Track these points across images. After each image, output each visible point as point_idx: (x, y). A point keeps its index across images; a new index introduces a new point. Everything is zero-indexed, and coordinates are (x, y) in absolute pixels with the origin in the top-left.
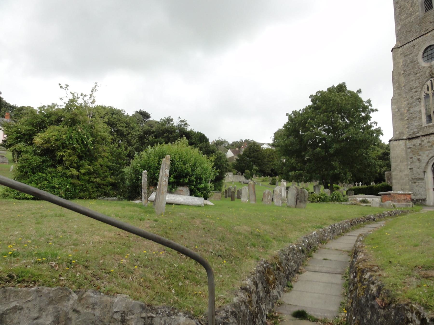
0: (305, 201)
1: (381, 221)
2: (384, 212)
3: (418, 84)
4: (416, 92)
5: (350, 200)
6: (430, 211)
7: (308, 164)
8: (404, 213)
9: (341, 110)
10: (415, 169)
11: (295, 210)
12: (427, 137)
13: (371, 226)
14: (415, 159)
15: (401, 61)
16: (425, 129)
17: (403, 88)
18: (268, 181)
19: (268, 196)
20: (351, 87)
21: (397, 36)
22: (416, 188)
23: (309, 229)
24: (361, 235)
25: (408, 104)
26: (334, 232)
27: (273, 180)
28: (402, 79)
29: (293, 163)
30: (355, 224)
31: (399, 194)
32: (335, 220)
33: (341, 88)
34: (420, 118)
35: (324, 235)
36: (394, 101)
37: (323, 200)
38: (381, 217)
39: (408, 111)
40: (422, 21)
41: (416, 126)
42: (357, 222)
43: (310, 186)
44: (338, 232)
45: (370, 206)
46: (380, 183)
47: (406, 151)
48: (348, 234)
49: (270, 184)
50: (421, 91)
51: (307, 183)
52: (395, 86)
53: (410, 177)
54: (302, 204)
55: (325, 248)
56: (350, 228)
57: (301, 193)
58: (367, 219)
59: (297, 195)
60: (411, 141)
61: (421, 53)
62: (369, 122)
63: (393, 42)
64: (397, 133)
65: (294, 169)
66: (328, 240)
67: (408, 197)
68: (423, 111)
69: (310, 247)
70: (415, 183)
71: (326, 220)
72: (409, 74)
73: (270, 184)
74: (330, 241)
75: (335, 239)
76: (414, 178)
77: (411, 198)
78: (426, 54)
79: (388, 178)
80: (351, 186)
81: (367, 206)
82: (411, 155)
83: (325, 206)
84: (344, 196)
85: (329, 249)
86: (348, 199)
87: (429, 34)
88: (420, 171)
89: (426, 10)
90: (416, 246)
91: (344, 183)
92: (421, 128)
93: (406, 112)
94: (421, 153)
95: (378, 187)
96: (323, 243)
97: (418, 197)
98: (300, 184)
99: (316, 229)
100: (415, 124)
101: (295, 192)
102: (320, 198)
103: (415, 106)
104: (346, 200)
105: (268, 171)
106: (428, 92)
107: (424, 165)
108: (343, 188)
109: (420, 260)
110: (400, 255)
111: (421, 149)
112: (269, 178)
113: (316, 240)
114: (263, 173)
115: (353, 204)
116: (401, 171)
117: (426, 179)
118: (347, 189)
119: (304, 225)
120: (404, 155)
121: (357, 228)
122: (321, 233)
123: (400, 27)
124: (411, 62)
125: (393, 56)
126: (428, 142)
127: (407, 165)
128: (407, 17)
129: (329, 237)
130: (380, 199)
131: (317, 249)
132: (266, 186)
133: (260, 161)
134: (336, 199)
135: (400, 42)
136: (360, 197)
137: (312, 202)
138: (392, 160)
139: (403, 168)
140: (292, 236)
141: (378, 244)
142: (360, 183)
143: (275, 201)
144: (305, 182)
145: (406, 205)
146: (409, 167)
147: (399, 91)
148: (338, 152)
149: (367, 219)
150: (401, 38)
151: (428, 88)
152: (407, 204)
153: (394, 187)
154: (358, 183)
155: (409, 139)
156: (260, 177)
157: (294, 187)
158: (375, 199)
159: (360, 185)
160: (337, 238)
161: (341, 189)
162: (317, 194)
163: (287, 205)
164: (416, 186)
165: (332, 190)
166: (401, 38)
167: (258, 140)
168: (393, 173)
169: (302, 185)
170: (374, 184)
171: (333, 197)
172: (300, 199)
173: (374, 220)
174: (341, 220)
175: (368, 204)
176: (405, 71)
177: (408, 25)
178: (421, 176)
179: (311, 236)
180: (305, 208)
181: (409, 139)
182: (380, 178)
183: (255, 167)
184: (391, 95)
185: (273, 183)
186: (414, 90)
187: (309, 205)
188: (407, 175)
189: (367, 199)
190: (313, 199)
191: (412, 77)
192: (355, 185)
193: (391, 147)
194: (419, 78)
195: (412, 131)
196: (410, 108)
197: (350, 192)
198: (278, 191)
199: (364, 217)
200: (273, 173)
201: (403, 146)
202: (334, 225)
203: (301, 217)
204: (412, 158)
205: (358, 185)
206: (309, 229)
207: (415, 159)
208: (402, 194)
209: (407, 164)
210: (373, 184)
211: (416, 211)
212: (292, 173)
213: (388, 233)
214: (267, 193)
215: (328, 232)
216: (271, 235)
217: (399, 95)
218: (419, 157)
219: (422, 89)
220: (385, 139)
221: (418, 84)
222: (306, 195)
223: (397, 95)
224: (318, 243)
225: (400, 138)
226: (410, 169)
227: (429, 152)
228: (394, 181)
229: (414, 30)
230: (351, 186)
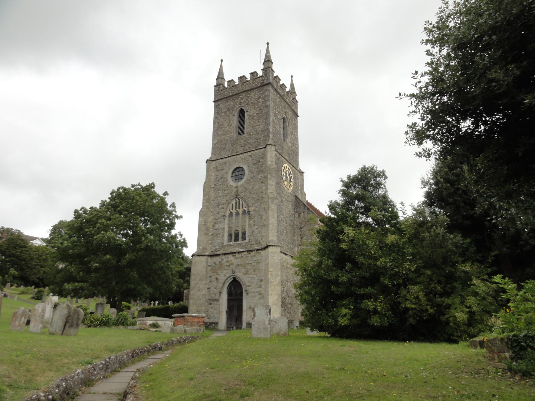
0: (78, 325)
1: (168, 349)
2: (173, 339)
3: (225, 201)
4: (222, 208)
5: (139, 324)
6: (218, 337)
7: (93, 275)
8: (193, 339)
9: (144, 213)
10: (212, 289)
11: (60, 339)
12: (227, 256)
13: (155, 357)
14: (213, 278)
15: (213, 174)
16: (226, 248)
17: (212, 202)
18: (31, 294)
19: (21, 318)
20: (159, 190)
21: (213, 149)
22: (211, 310)
23: (73, 367)
24: (138, 370)
25: (215, 219)
26: (107, 368)
27: (39, 292)
28: (212, 193)
29: (72, 272)
30: (136, 355)
31: (193, 317)
32: (112, 351)
33: (149, 190)
34: (223, 236)
35: (92, 375)
36: (202, 214)
37: (105, 323)
38: (169, 344)
39: (213, 226)
40: (234, 143)
41: (218, 243)
42: (141, 352)
43: (91, 304)
44: (111, 369)
45: (160, 331)
46: (178, 302)
47: (207, 268)
48: (125, 370)
49: (33, 298)
50: (226, 208)
51: (89, 299)
52: (205, 198)
53: (207, 297)
54: (72, 330)
55: (90, 393)
56: (130, 361)
57: (74, 313)
58: (153, 349)
59: (68, 317)
60: (212, 258)
61: (231, 172)
62: (173, 232)
63: (208, 154)
64: (201, 248)
65: (71, 279)
66: (97, 381)
67: (201, 320)
68: (226, 229)
69: (68, 394)
70: (211, 304)
71: (101, 351)
72: (219, 190)
73: (33, 298)
74: (100, 382)
75: (107, 378)
76: (210, 298)
77: (203, 322)
78: (234, 174)
79: (186, 296)
80: (146, 306)
81: (156, 331)
82: (210, 274)
83: (105, 331)
84: (134, 318)
85: (94, 393)
86: (136, 322)
87: (239, 156)
88: (217, 291)
89: (239, 134)
90: (191, 379)
91: (138, 302)
92: (222, 246)
93: (211, 227)
94: (219, 272)
95: (176, 307)
96: (89, 386)
97: (212, 320)
98: (79, 301)
99: (83, 365)
100: (218, 241)
101: (65, 312)
102: (101, 320)
103: (220, 222)
104: (134, 324)
105: (33, 278)
106: (232, 211)
107: (221, 285)
108: (136, 308)
109: (190, 396)
110: (172, 392)
111: (220, 268)
112: (33, 290)
113: (80, 382)
114: (24, 280)
115: (141, 329)
116: (199, 291)
117: (221, 300)
118: (140, 309)
119: (66, 361)
120: (204, 273)
121: (139, 361)
122: (89, 372)
123: (216, 142)
124: (222, 178)
125: (207, 167)
126: (227, 261)
127: (206, 284)
128: (223, 134)
129: (99, 376)
130: (172, 323)
131: (77, 396)
132: (24, 301)
133: (24, 262)
134: (121, 322)
135: (215, 155)
136: (150, 320)
137: (89, 326)
138: (192, 277)
139: (202, 286)
140: (42, 379)
141: (154, 380)
142: (157, 302)
143: (31, 324)
144: (86, 298)
145: (197, 329)
146: (207, 287)
147: (208, 204)
148: (131, 264)
149: (153, 349)
150: (216, 152)
151: (233, 206)
152: (199, 328)
153: (190, 308)
154: (154, 301)
155: (211, 256)
156: (19, 286)
157: (65, 305)
158: (167, 322)
159: (157, 305)
160: (110, 376)
161: (133, 308)
162: (98, 315)
163: (49, 330)
164: (212, 308)
165: (120, 310)
166: (216, 152)
167: (27, 232)
168: (191, 292)
169: (82, 302)
170: (172, 304)
171: (118, 320)
172: (70, 322)
173: (160, 349)
174: (121, 351)
175: (158, 329)
176: (215, 185)
177: (224, 141)
178: (217, 297)
179: (73, 377)
180: (75, 335)
181: (211, 256)
182: (178, 297)
183: (12, 271)
184: (200, 206)
185: (39, 297)
186: (221, 206)
187: (83, 330)
188: (204, 295)
189: (158, 322)
190: (92, 322)
191: (220, 193)
192: (151, 304)
193: (193, 261)
194: (226, 196)
195: (214, 248)
196: (215, 223)
197: (142, 312)
198: (40, 310)
199: (150, 345)
200: (40, 283)
201: (204, 263)
202: (109, 358)
203: (66, 349)
204: (210, 276)
205: (154, 304)
206: (73, 367)
207: (213, 278)
208: (196, 317)
209: (206, 283)
210: (170, 303)
211: (206, 337)
212: (68, 286)
213: (169, 365)
214: (20, 312)
215: (99, 369)
216: (7, 379)
217: (208, 208)
218: (217, 276)
219: (227, 206)
220: (188, 252)
221: (225, 201)
222: (80, 317)
223: (205, 208)
224: (82, 387)
225: (203, 254)
226: (208, 288)
227: (226, 271)
228: (191, 301)
229: (227, 148)
230: (146, 306)
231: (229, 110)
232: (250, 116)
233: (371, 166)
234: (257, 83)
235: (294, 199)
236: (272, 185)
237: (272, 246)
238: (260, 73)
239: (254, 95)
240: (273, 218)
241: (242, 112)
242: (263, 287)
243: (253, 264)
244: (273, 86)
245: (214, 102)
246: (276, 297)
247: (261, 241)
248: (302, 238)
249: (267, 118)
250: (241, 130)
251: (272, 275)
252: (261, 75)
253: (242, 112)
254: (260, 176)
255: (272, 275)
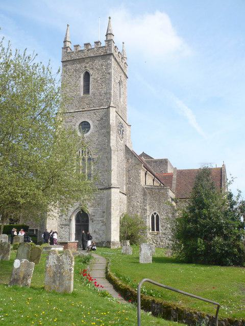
160: (229, 265)
231: (76, 70)
232: (95, 79)
233: (220, 166)
234: (101, 52)
235: (124, 147)
236: (113, 140)
237: (114, 188)
238: (103, 44)
239: (98, 63)
240: (114, 166)
241: (87, 76)
242: (105, 217)
243: (97, 200)
244: (114, 56)
245: (62, 62)
246: (116, 225)
247: (104, 183)
248: (129, 178)
249: (109, 84)
250: (87, 90)
251: (114, 210)
252: (104, 45)
253: (87, 76)
254: (103, 130)
255: (113, 209)
